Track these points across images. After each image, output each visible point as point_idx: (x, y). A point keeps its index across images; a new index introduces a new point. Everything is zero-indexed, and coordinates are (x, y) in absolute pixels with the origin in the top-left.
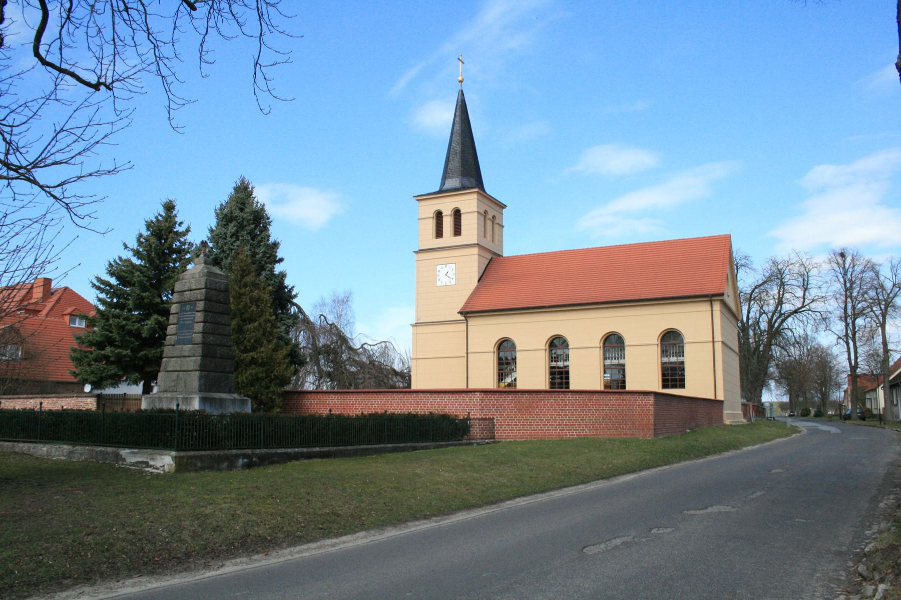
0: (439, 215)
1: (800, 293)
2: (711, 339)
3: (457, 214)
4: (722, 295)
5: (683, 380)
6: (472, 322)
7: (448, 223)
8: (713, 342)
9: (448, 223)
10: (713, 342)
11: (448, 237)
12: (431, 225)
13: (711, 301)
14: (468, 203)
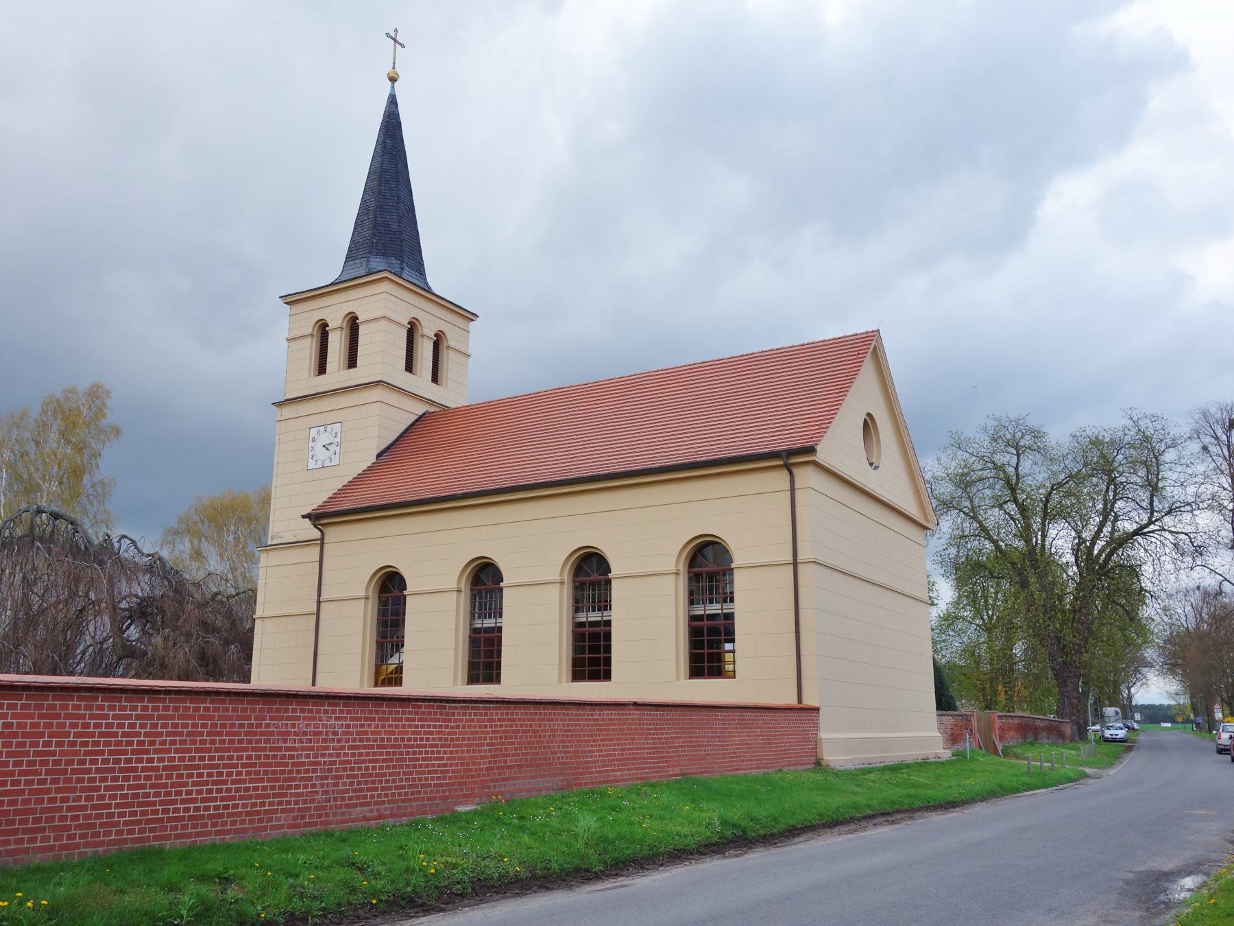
0: (323, 330)
1: (1144, 495)
2: (790, 558)
3: (353, 325)
4: (811, 450)
5: (608, 661)
6: (332, 534)
7: (337, 344)
8: (795, 564)
9: (337, 344)
10: (795, 564)
11: (337, 374)
12: (309, 348)
13: (789, 468)
14: (382, 305)
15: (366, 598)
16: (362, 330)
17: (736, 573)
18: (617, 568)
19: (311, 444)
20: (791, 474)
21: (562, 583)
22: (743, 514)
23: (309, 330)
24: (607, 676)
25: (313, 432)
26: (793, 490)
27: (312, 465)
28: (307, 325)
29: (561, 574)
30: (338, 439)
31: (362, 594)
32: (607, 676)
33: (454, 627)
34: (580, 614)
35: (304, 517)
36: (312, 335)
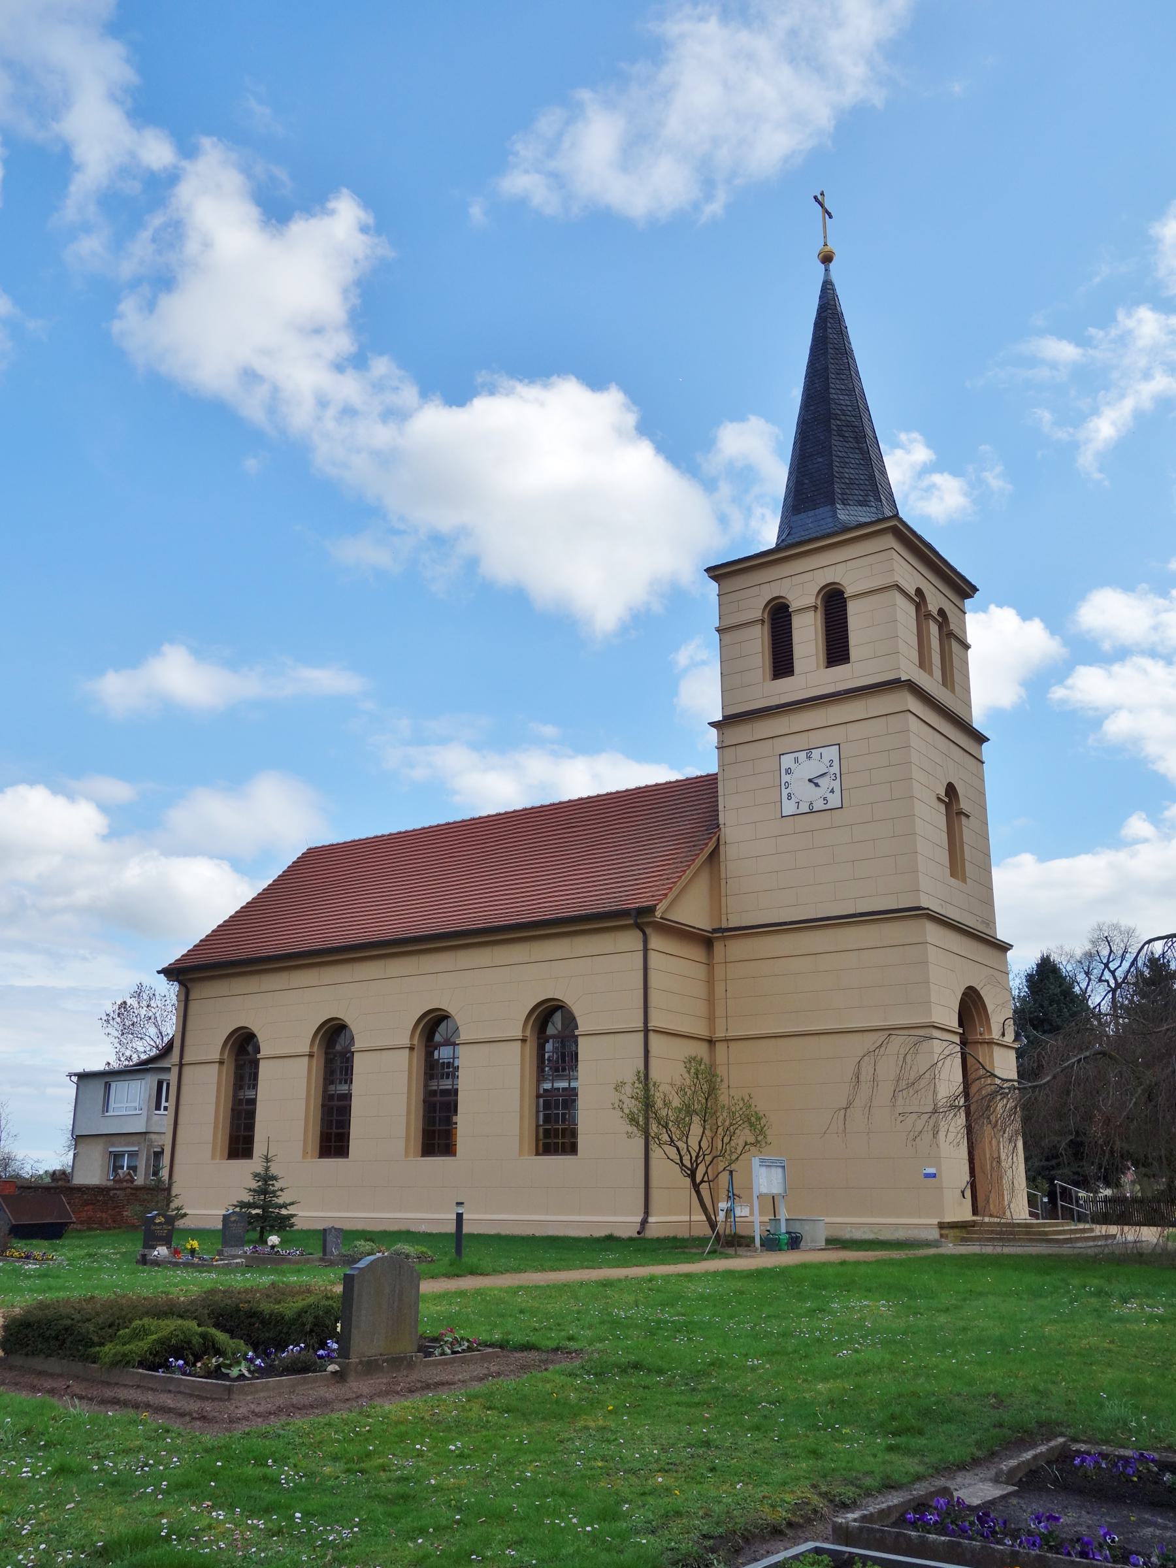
3: (834, 603)
5: (574, 1133)
7: (807, 634)
9: (807, 634)
11: (811, 673)
12: (757, 641)
13: (640, 927)
15: (524, 1041)
16: (853, 608)
17: (581, 1040)
18: (266, 1049)
19: (785, 778)
20: (644, 934)
21: (524, 1041)
22: (596, 979)
23: (758, 614)
24: (572, 1149)
25: (787, 761)
26: (646, 950)
27: (789, 808)
28: (755, 607)
29: (222, 1053)
30: (835, 769)
31: (519, 1034)
32: (572, 1149)
33: (518, 1085)
34: (332, 1087)
35: (159, 972)
36: (763, 621)
